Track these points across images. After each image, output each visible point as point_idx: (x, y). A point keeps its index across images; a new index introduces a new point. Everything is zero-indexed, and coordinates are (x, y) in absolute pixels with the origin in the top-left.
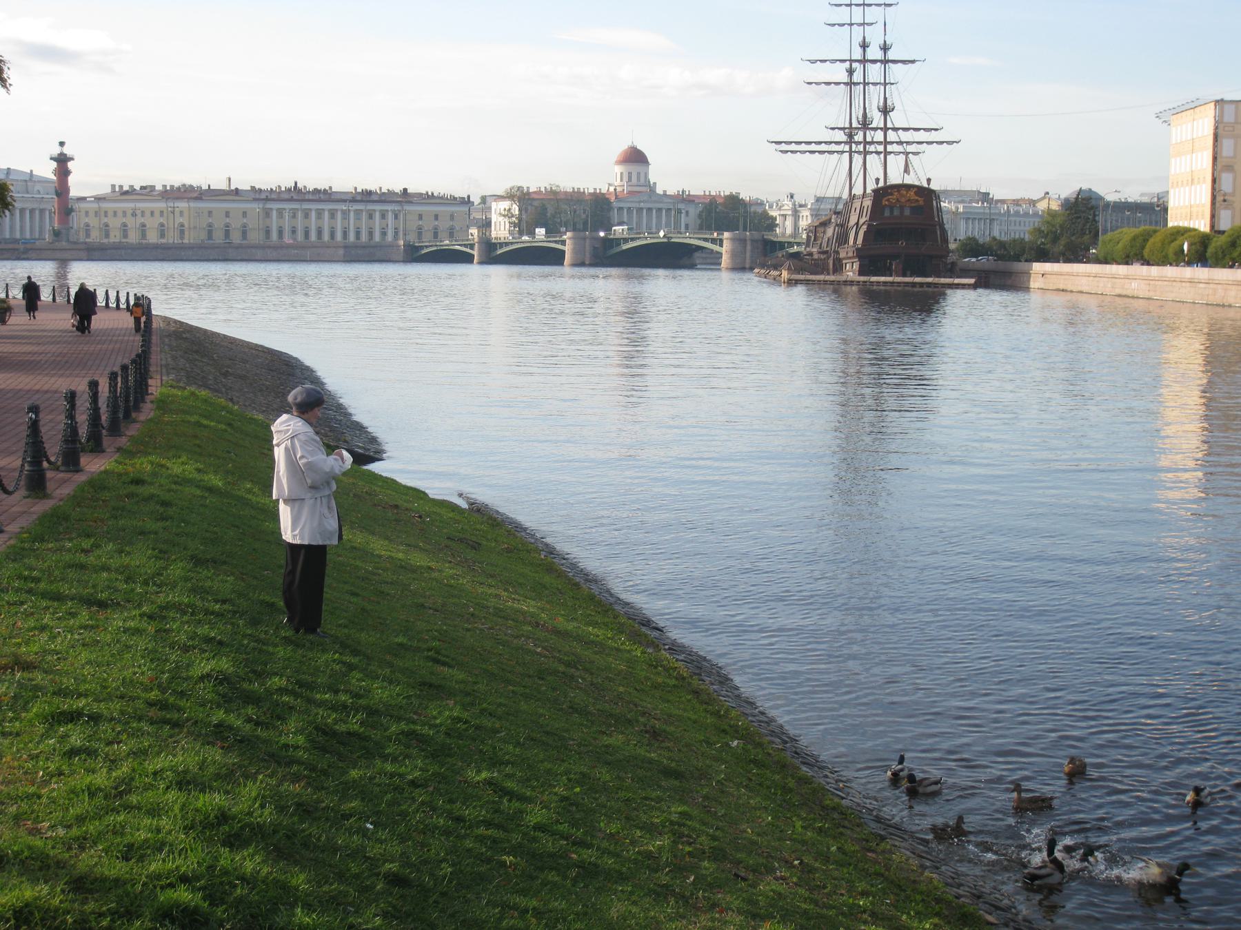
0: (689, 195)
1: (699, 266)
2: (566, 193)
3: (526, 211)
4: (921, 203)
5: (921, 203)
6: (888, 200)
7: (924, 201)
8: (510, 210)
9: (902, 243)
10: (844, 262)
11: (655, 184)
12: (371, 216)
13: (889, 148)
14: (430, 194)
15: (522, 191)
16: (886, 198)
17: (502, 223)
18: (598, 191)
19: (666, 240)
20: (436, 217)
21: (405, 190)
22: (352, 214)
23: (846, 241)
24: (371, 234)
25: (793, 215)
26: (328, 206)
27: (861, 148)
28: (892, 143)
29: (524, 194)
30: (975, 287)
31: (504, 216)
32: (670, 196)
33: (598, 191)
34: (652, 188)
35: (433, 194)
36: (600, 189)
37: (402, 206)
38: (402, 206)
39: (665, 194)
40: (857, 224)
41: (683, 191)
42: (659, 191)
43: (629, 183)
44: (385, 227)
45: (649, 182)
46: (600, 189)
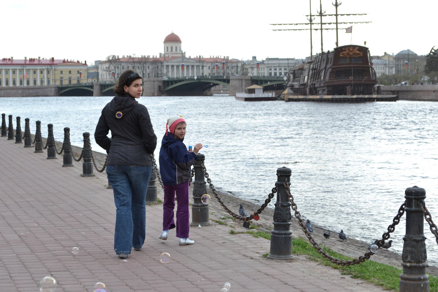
0: (203, 58)
1: (214, 95)
2: (139, 58)
3: (118, 68)
4: (361, 55)
5: (361, 55)
6: (343, 54)
7: (363, 54)
8: (109, 68)
9: (351, 78)
10: (318, 89)
11: (185, 52)
12: (35, 72)
13: (324, 26)
14: (66, 60)
15: (115, 58)
16: (341, 53)
17: (105, 75)
18: (155, 57)
19: (198, 81)
20: (70, 72)
21: (53, 58)
22: (25, 71)
23: (319, 77)
24: (35, 82)
25: (256, 67)
26: (11, 68)
27: (319, 27)
28: (325, 24)
29: (117, 60)
30: (229, 96)
31: (106, 71)
32: (192, 59)
33: (155, 57)
34: (183, 55)
35: (67, 60)
36: (156, 56)
37: (52, 67)
38: (52, 67)
39: (190, 58)
40: (325, 68)
41: (200, 56)
42: (187, 56)
43: (172, 52)
44: (43, 78)
45: (182, 51)
46: (156, 56)
